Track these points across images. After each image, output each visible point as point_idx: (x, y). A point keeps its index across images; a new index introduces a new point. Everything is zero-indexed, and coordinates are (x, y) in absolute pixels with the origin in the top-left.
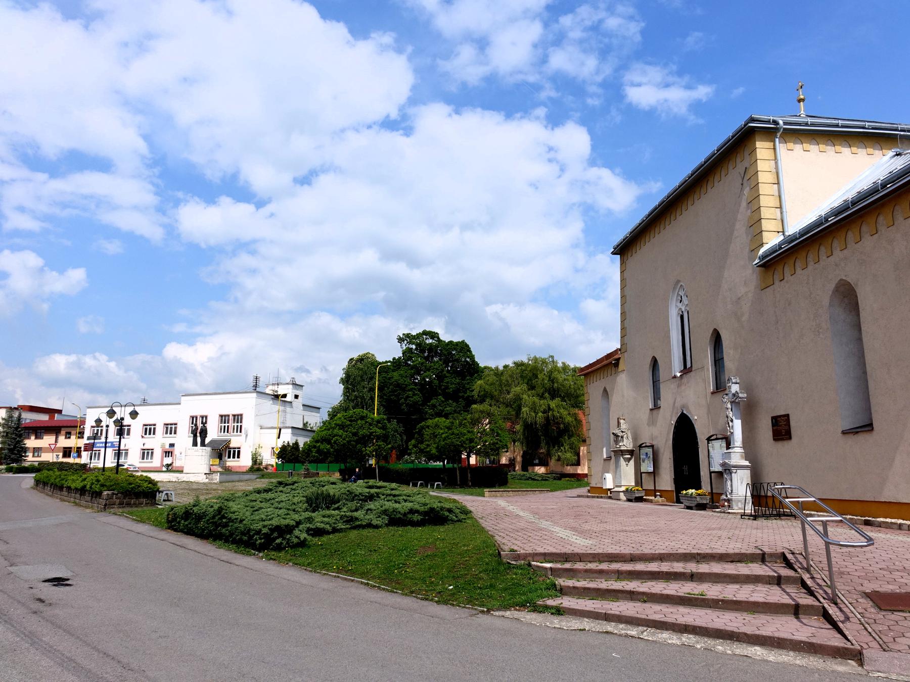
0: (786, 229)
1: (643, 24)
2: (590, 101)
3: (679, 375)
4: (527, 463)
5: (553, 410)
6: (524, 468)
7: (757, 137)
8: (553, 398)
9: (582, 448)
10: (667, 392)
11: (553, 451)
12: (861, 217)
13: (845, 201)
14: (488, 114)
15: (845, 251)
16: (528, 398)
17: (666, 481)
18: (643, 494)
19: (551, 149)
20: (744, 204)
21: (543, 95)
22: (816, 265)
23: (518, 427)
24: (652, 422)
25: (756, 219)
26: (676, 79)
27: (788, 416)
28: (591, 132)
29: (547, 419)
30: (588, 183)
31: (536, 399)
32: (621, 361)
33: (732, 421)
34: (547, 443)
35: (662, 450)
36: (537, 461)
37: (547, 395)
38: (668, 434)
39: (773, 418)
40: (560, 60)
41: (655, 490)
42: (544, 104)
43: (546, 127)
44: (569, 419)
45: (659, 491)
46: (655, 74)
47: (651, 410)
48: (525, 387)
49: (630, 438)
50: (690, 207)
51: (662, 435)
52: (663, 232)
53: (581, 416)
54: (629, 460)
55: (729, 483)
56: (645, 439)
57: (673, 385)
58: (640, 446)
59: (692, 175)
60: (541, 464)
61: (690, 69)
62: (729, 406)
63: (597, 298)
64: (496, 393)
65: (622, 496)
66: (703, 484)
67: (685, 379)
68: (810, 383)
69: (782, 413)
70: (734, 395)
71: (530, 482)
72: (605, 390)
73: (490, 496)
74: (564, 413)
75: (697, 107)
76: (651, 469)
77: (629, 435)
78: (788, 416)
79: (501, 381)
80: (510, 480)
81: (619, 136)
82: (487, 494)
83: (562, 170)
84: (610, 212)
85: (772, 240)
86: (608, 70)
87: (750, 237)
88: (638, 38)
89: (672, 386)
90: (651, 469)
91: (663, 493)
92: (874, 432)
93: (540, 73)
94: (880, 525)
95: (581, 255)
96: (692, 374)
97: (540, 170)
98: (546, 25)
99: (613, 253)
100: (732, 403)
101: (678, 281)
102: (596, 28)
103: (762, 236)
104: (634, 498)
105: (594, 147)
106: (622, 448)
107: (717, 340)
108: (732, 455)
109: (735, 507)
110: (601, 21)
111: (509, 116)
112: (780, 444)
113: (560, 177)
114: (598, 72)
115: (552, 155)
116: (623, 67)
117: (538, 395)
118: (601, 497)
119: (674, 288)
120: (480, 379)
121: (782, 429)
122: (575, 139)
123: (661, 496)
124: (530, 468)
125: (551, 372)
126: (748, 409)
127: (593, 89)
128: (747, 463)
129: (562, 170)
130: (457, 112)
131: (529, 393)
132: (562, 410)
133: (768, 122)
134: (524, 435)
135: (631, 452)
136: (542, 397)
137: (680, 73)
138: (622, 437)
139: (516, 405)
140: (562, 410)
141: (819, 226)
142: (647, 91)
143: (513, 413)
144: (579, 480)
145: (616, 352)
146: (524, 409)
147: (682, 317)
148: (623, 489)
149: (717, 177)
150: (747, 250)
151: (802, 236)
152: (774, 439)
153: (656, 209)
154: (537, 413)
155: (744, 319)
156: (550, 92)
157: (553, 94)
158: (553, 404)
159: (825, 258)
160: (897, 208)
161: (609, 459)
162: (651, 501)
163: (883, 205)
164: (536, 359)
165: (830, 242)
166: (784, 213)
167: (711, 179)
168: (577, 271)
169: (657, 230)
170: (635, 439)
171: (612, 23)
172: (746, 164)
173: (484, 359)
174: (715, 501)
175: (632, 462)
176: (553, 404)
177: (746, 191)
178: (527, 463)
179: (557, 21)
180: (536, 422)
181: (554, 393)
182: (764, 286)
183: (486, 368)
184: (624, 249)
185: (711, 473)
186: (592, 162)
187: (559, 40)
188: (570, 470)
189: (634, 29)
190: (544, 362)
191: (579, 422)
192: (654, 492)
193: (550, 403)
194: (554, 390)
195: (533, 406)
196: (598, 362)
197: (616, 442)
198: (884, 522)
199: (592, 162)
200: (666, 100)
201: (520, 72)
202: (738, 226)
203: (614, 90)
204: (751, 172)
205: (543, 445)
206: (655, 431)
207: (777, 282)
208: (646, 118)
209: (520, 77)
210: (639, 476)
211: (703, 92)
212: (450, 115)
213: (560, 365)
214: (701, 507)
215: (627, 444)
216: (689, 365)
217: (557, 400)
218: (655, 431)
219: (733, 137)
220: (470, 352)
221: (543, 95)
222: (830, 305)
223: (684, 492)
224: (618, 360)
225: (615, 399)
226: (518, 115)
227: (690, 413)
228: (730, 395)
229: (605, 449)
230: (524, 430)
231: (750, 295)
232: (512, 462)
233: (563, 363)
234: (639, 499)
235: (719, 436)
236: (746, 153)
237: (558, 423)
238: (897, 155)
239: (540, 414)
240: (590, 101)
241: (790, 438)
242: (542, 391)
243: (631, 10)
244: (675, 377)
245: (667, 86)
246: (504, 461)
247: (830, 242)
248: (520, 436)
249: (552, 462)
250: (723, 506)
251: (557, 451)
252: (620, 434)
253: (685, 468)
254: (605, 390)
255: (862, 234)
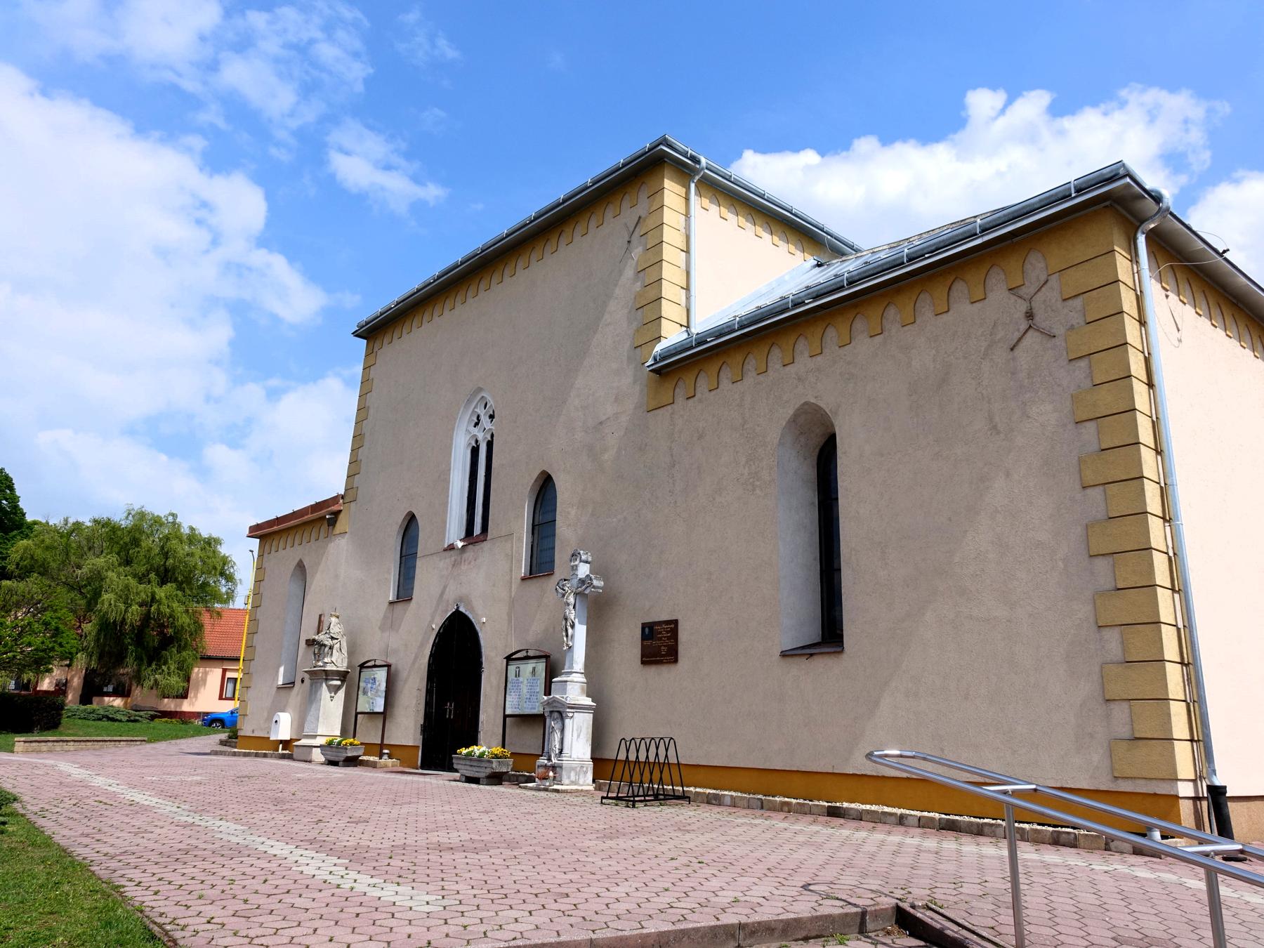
0: (692, 324)
1: (371, 71)
2: (273, 151)
3: (460, 544)
4: (91, 691)
5: (159, 602)
6: (85, 699)
7: (667, 172)
8: (163, 582)
9: (196, 670)
10: (427, 575)
11: (147, 672)
12: (856, 306)
13: (783, 298)
14: (102, 113)
15: (819, 358)
16: (116, 578)
17: (407, 729)
18: (361, 752)
19: (205, 205)
20: (629, 272)
21: (204, 117)
22: (761, 378)
23: (87, 627)
24: (389, 624)
25: (652, 295)
26: (402, 162)
27: (676, 622)
28: (269, 197)
29: (146, 618)
30: (250, 269)
31: (132, 582)
32: (341, 516)
33: (573, 626)
34: (139, 659)
35: (403, 675)
36: (110, 688)
37: (152, 576)
38: (422, 645)
39: (644, 626)
40: (239, 74)
41: (382, 746)
42: (200, 131)
43: (201, 170)
44: (184, 620)
45: (390, 746)
46: (376, 146)
47: (391, 603)
48: (114, 558)
49: (345, 650)
50: (519, 271)
51: (411, 644)
52: (459, 307)
53: (206, 619)
54: (338, 688)
55: (557, 736)
56: (371, 652)
57: (445, 563)
58: (362, 666)
59: (439, 277)
60: (117, 693)
61: (425, 155)
62: (571, 600)
63: (234, 445)
64: (54, 565)
65: (317, 755)
66: (481, 736)
67: (470, 553)
68: (740, 562)
69: (665, 617)
70: (582, 581)
71: (105, 723)
72: (301, 567)
73: (26, 752)
74: (178, 608)
75: (418, 207)
76: (379, 708)
77: (344, 644)
78: (676, 622)
79: (68, 546)
80: (64, 720)
81: (308, 217)
82: (19, 747)
83: (216, 241)
84: (276, 319)
85: (672, 336)
86: (309, 114)
87: (635, 325)
88: (359, 88)
89: (441, 564)
90: (379, 708)
91: (396, 751)
92: (844, 656)
93: (205, 83)
94: (859, 817)
95: (220, 380)
96: (486, 546)
97: (175, 231)
98: (228, 13)
99: (357, 334)
100: (576, 594)
101: (480, 390)
102: (302, 49)
103: (660, 325)
104: (339, 757)
105: (269, 223)
106: (329, 668)
107: (545, 489)
108: (569, 686)
109: (565, 781)
110: (312, 42)
111: (141, 129)
112: (652, 670)
113: (207, 251)
114: (292, 114)
115: (203, 214)
116: (330, 120)
117: (135, 576)
118: (265, 756)
119: (469, 401)
120: (27, 537)
121: (660, 644)
122: (243, 203)
123: (390, 756)
124: (95, 699)
125: (167, 538)
126: (599, 609)
127: (282, 135)
128: (588, 701)
129: (216, 241)
130: (44, 93)
131: (121, 569)
132: (175, 605)
133: (685, 154)
134: (97, 640)
135: (343, 676)
136: (141, 579)
137: (408, 156)
138: (331, 648)
139: (91, 589)
140: (175, 605)
141: (680, 352)
142: (360, 164)
143: (83, 602)
144: (184, 723)
145: (334, 500)
146: (105, 596)
147: (475, 452)
148: (321, 741)
149: (580, 229)
150: (627, 345)
151: (742, 327)
152: (643, 663)
153: (456, 266)
154: (128, 605)
155: (606, 457)
156: (212, 116)
157: (221, 123)
158: (161, 593)
159: (778, 366)
160: (702, 375)
161: (289, 685)
162: (373, 765)
163: (898, 291)
164: (142, 515)
165: (791, 342)
166: (692, 298)
167: (568, 230)
168: (208, 399)
169: (448, 304)
170: (351, 653)
171: (327, 52)
172: (641, 210)
173: (36, 505)
174: (526, 768)
175: (341, 693)
176: (161, 593)
177: (637, 252)
178: (91, 691)
179: (243, 13)
180: (124, 621)
181: (165, 576)
182: (653, 404)
183: (35, 523)
184: (375, 331)
185: (505, 716)
186: (263, 242)
187: (244, 45)
188: (169, 705)
189: (357, 72)
190: (157, 521)
191: (199, 627)
192: (379, 749)
193: (157, 590)
194: (166, 570)
195: (122, 594)
196: (295, 515)
197: (318, 656)
198: (868, 812)
199: (263, 242)
200: (383, 189)
201: (172, 68)
202: (612, 306)
203: (312, 147)
204: (651, 223)
205: (130, 660)
206: (395, 640)
207: (680, 400)
208: (355, 204)
209: (169, 76)
210: (351, 719)
211: (433, 192)
212: (32, 95)
213: (185, 530)
214: (496, 779)
215: (337, 661)
216: (477, 530)
217: (170, 587)
218: (395, 640)
219: (462, 263)
220: (11, 488)
221: (204, 117)
222: (781, 444)
223: (464, 751)
224: (338, 513)
225: (318, 582)
226: (157, 134)
227: (472, 610)
228: (575, 582)
229: (282, 669)
230: (99, 631)
231: (624, 419)
232: (61, 688)
233: (192, 529)
234: (352, 762)
235: (531, 653)
236: (643, 196)
237: (162, 626)
238: (819, 265)
239: (135, 607)
240: (273, 151)
241: (676, 661)
242: (143, 569)
243: (358, 45)
244: (451, 547)
245: (388, 167)
246: (46, 684)
247: (791, 342)
248: (90, 642)
249: (137, 692)
250: (545, 778)
251: (155, 671)
252: (329, 642)
253: (450, 706)
254: (301, 567)
255: (951, 301)
